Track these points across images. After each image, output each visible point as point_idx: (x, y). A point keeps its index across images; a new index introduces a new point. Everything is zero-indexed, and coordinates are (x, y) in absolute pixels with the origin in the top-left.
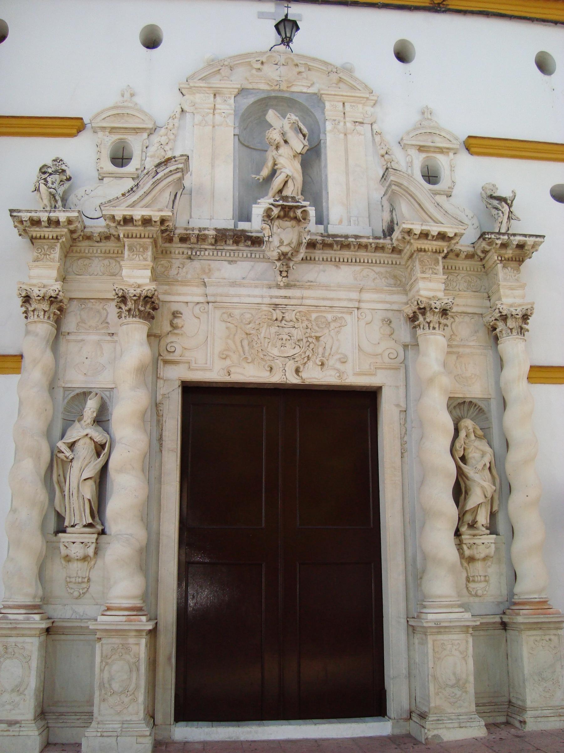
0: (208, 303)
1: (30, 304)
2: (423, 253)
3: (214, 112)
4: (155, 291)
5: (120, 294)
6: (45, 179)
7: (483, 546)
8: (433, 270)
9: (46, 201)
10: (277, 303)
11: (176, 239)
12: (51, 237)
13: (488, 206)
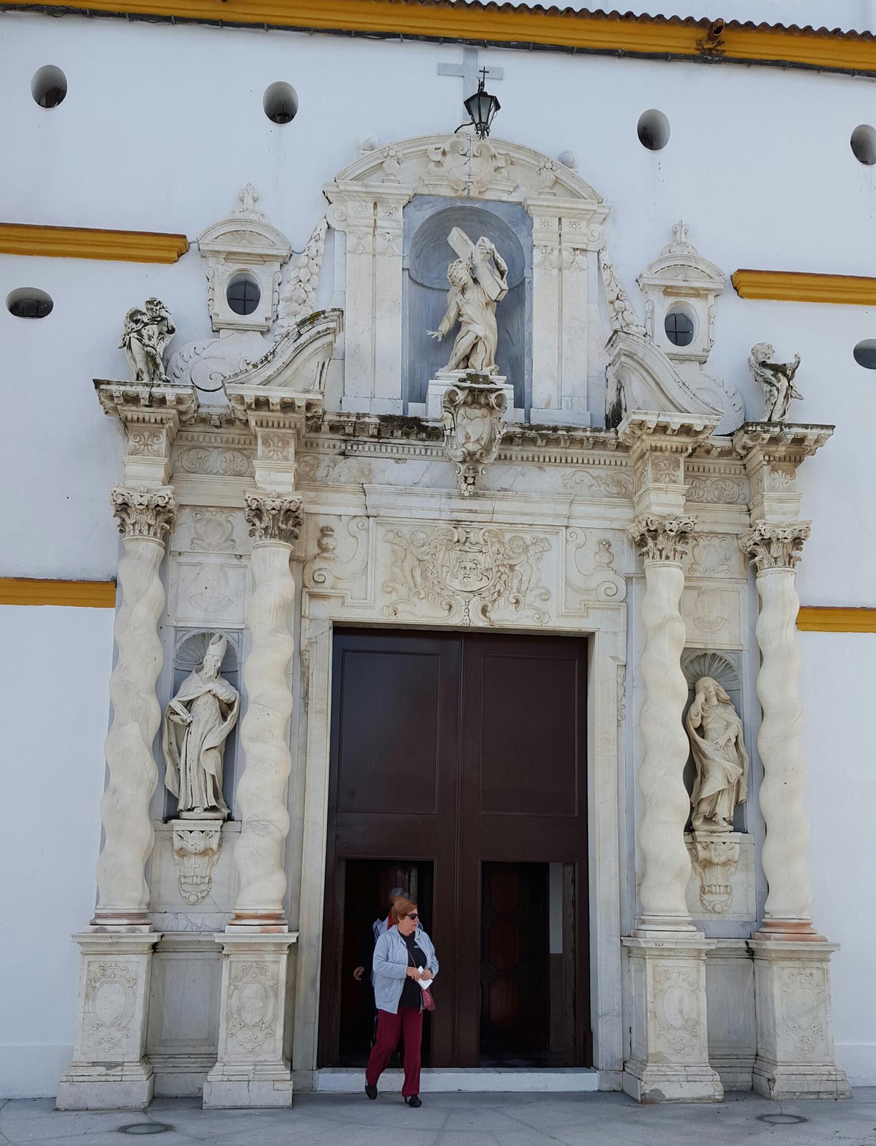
0: (368, 517)
1: (128, 514)
2: (658, 454)
3: (374, 232)
4: (301, 503)
5: (254, 507)
6: (139, 332)
7: (723, 846)
8: (671, 476)
9: (141, 365)
10: (459, 519)
11: (325, 428)
12: (153, 420)
13: (758, 378)
